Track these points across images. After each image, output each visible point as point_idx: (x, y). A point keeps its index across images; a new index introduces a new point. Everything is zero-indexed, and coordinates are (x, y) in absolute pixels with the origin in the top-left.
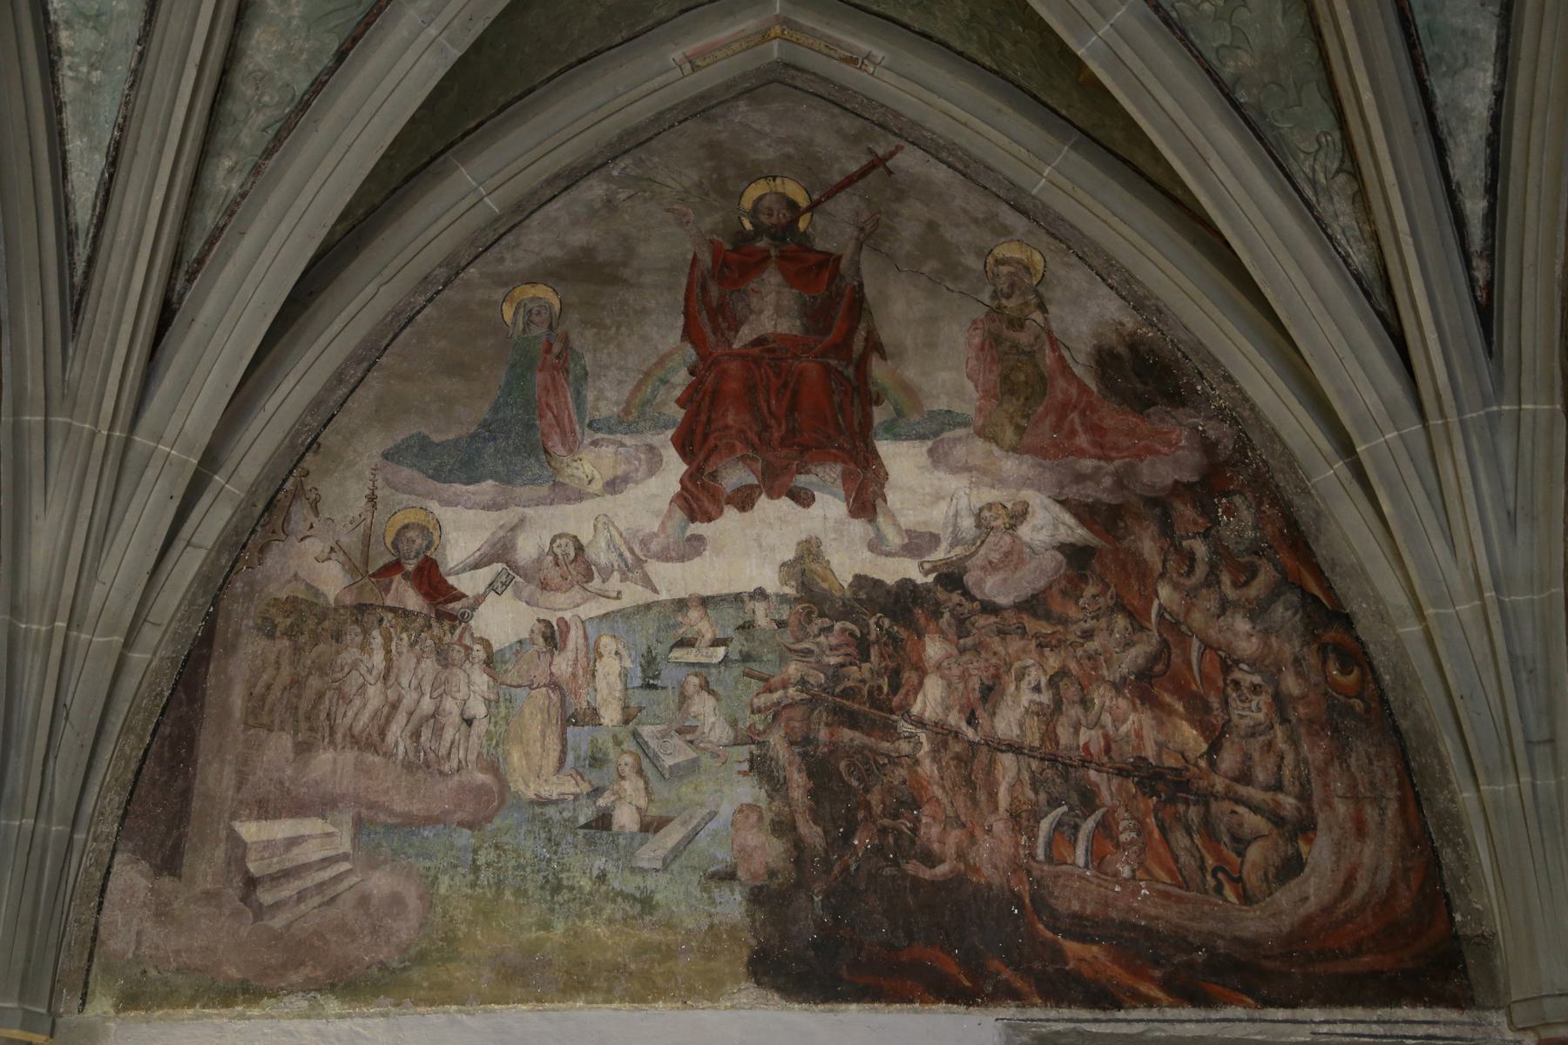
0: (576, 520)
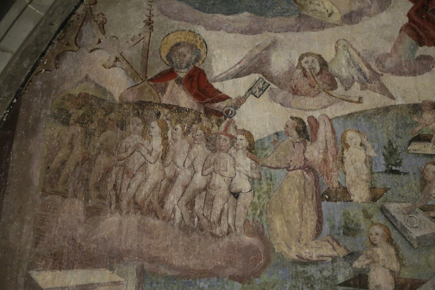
0: (322, 43)
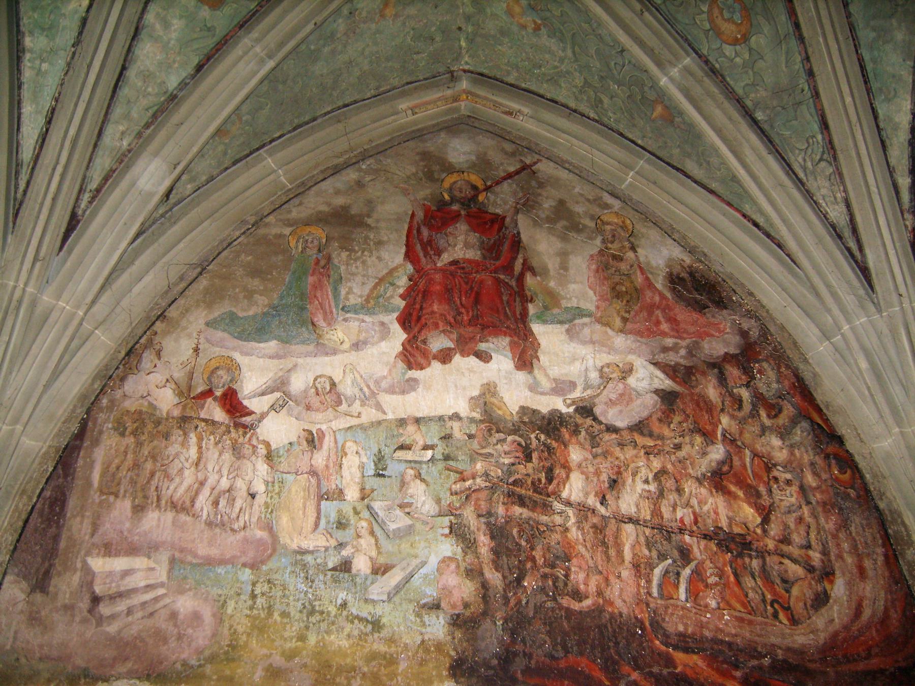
0: (330, 366)
